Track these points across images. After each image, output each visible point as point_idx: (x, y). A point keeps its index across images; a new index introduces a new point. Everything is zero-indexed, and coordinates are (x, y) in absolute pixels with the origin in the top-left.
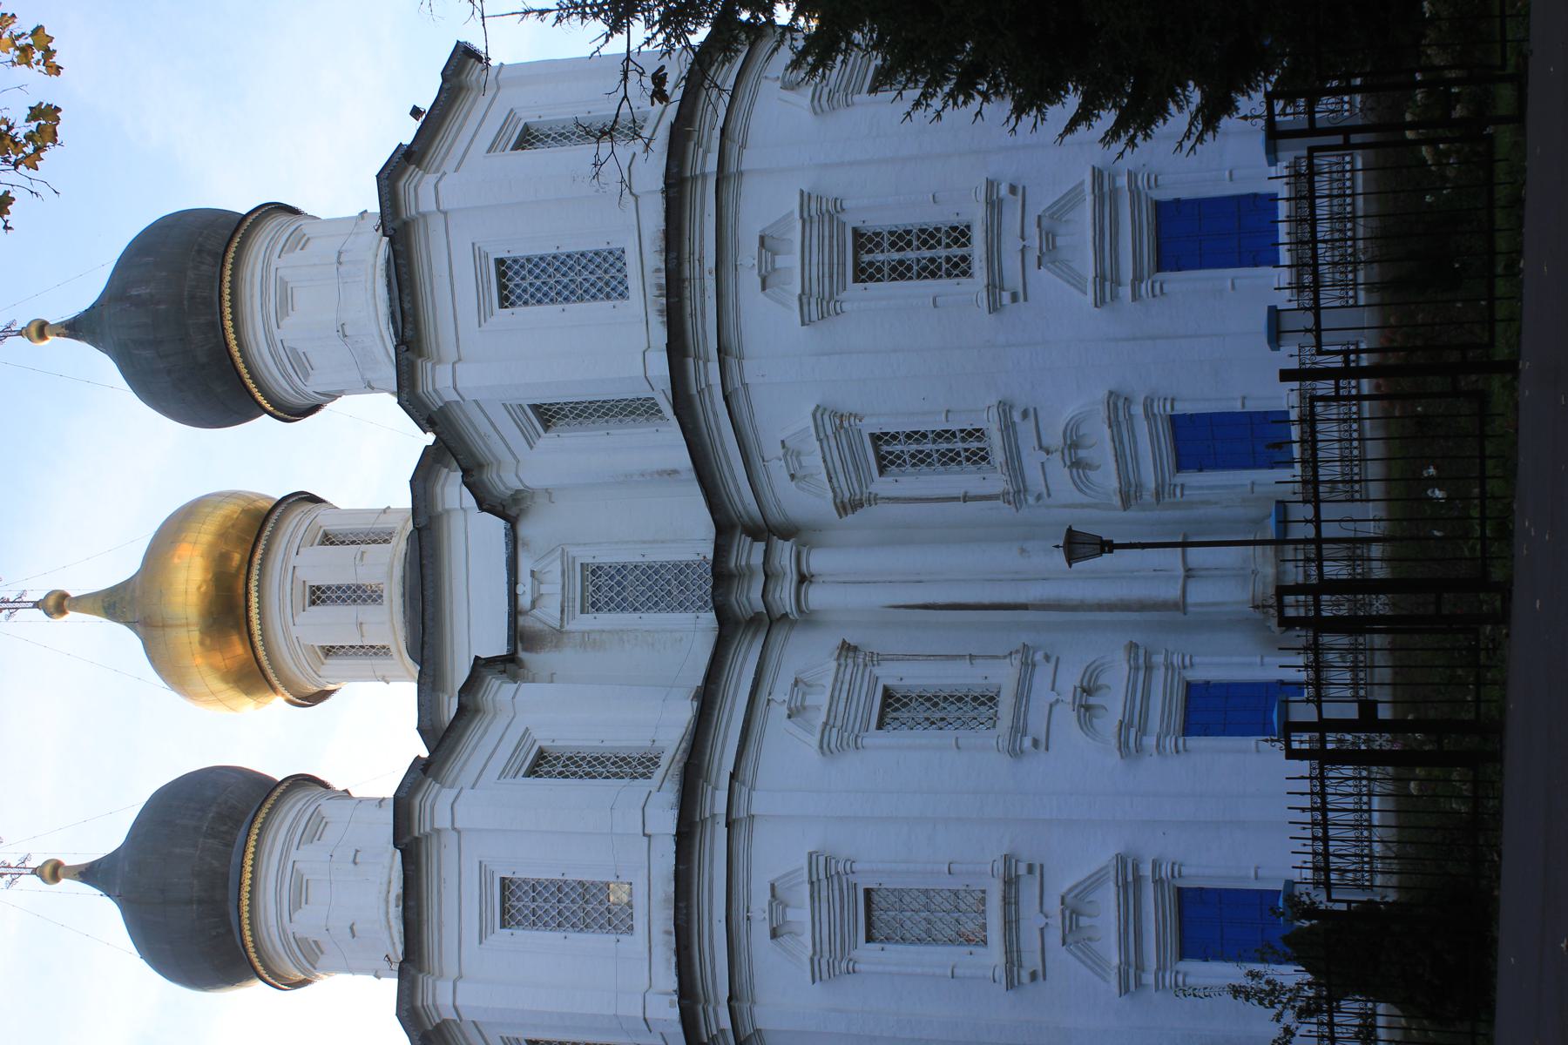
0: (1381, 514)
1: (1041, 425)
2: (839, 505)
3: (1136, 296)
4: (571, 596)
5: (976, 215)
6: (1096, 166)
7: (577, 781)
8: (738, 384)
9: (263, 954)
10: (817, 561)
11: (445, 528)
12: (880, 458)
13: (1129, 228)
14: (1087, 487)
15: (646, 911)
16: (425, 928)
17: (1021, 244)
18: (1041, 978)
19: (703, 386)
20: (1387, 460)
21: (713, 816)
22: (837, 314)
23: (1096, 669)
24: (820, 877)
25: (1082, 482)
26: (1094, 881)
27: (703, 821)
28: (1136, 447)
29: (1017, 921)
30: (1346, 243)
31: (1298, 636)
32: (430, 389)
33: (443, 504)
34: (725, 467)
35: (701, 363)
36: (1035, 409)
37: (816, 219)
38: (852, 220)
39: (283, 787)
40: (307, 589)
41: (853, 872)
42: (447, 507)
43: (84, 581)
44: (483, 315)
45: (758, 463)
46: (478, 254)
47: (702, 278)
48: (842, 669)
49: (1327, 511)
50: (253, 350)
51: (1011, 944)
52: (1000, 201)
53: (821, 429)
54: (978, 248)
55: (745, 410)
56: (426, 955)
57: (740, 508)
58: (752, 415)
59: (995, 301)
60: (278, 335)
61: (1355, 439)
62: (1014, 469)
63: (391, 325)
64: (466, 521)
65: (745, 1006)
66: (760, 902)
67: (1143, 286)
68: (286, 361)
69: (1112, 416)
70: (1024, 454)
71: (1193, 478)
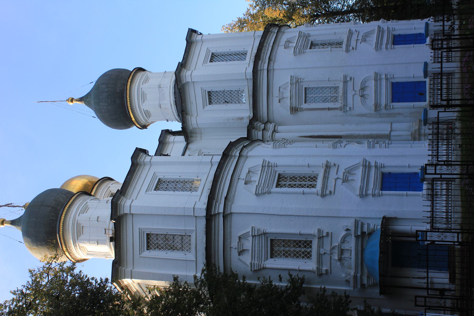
1: (355, 83)
2: (291, 108)
3: (387, 48)
5: (341, 85)
6: (376, 72)
8: (272, 68)
9: (64, 226)
10: (280, 128)
11: (166, 147)
13: (386, 37)
14: (364, 104)
15: (204, 183)
16: (130, 187)
18: (333, 193)
19: (262, 69)
22: (304, 53)
23: (364, 81)
24: (266, 165)
25: (364, 102)
28: (381, 90)
29: (328, 178)
30: (448, 191)
32: (184, 74)
35: (263, 63)
36: (354, 78)
37: (302, 36)
38: (311, 39)
40: (111, 193)
42: (169, 141)
44: (204, 62)
45: (271, 95)
46: (208, 50)
47: (268, 47)
50: (133, 90)
51: (325, 183)
53: (292, 81)
56: (126, 195)
59: (348, 48)
60: (141, 86)
61: (450, 201)
62: (345, 97)
63: (174, 83)
64: (173, 145)
65: (230, 203)
66: (245, 171)
67: (389, 45)
68: (140, 96)
69: (376, 76)
70: (348, 92)
71: (396, 105)
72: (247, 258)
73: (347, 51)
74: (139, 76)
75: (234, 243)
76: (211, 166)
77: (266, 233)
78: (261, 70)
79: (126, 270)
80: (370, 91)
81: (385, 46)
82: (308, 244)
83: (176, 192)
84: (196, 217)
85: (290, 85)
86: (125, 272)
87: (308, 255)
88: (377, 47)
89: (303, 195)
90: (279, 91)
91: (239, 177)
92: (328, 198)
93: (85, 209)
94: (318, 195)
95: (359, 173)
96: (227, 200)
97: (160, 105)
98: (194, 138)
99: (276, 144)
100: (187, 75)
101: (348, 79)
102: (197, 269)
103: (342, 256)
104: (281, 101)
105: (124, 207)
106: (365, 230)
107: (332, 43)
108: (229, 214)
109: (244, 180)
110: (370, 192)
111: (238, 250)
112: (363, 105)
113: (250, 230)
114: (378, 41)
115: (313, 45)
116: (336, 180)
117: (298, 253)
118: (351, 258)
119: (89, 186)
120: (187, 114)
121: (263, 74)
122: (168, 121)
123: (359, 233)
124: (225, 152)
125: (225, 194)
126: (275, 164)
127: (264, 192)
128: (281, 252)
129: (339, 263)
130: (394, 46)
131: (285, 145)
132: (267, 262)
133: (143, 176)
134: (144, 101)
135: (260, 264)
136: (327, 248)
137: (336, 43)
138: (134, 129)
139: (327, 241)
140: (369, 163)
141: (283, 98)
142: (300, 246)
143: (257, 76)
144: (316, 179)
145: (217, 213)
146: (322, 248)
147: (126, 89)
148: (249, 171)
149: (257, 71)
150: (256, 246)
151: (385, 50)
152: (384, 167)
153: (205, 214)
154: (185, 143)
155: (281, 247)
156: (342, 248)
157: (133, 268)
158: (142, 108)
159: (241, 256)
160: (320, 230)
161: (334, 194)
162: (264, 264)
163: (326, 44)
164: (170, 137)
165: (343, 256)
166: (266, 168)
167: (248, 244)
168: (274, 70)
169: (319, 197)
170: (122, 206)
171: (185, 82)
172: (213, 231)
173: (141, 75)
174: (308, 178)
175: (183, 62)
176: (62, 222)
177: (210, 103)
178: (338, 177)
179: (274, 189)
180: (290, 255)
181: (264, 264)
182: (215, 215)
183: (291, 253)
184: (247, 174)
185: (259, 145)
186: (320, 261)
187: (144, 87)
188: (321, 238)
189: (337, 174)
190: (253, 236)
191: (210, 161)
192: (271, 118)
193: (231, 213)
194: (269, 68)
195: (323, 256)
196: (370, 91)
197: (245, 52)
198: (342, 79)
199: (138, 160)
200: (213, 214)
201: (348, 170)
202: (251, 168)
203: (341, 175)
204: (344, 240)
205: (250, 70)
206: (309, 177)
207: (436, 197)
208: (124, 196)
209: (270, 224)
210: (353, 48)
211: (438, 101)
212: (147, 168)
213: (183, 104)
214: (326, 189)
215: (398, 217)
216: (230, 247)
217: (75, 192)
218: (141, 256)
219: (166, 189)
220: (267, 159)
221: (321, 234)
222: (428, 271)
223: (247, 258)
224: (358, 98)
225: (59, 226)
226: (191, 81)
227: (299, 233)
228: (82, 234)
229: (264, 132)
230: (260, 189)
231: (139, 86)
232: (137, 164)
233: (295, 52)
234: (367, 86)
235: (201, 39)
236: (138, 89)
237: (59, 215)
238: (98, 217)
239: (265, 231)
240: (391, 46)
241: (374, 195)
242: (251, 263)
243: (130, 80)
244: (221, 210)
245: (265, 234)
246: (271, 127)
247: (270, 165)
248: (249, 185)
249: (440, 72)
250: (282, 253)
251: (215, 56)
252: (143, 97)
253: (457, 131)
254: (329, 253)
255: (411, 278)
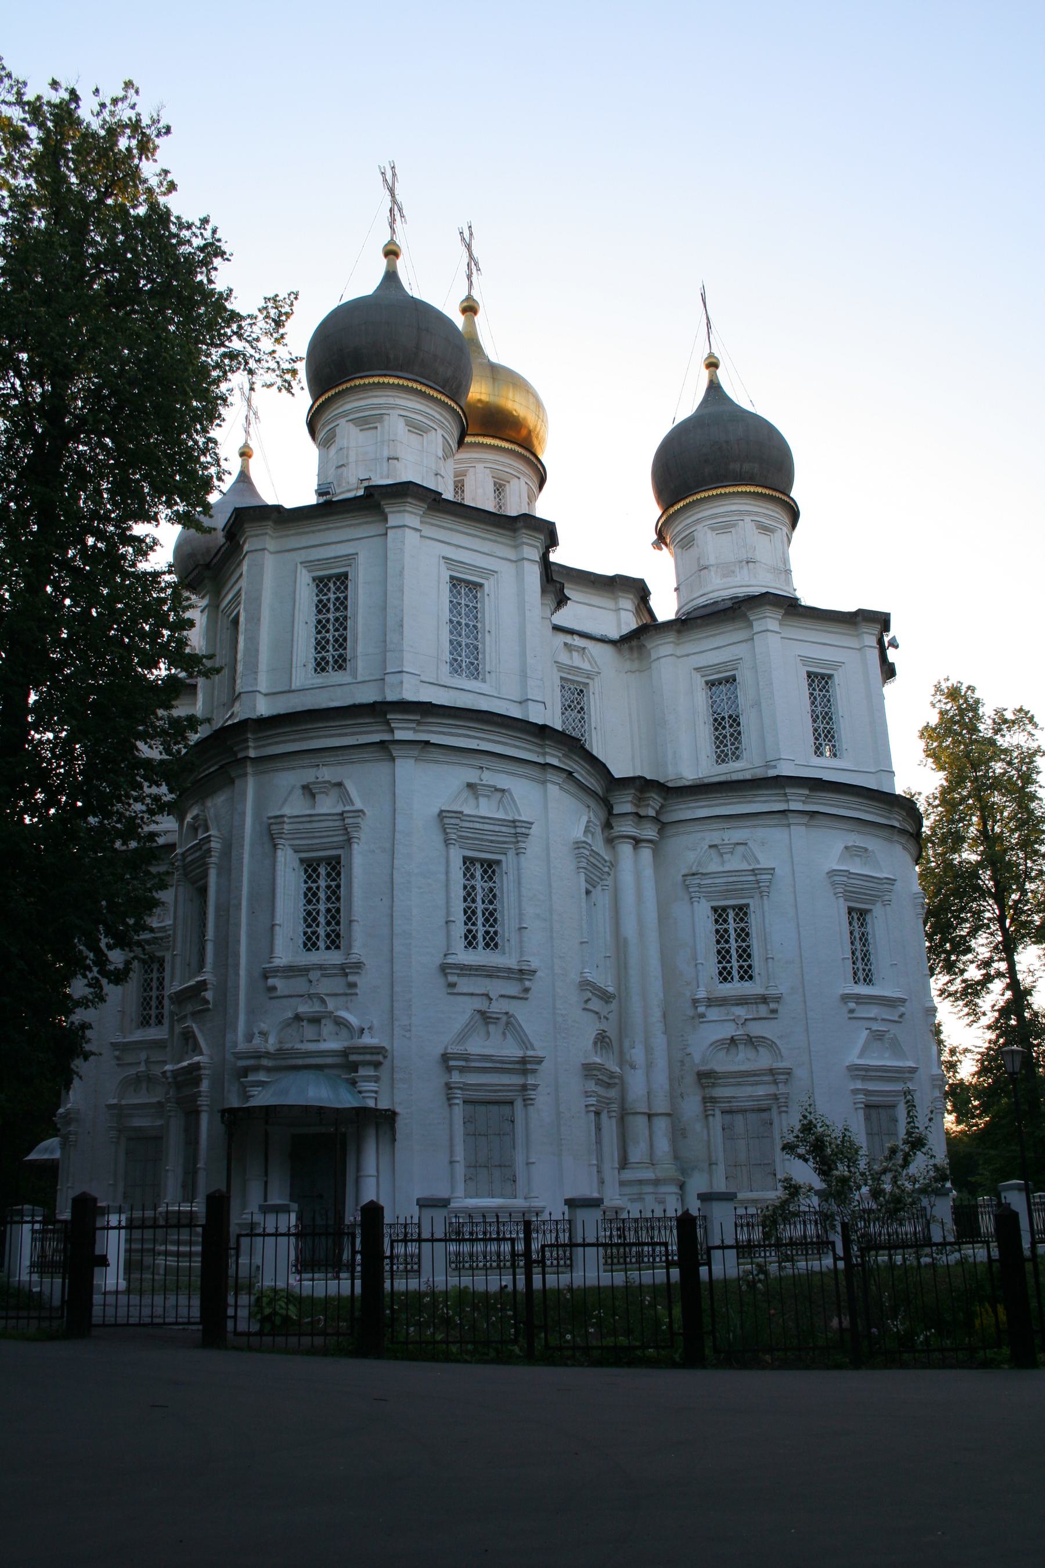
0: (589, 1283)
3: (855, 1092)
4: (572, 672)
7: (807, 693)
12: (724, 909)
17: (880, 1018)
19: (789, 797)
20: (570, 1289)
21: (544, 754)
22: (835, 894)
26: (524, 1043)
27: (542, 746)
31: (564, 1214)
33: (623, 597)
34: (722, 801)
35: (804, 798)
36: (776, 1018)
39: (786, 499)
41: (517, 854)
43: (723, 376)
44: (805, 660)
48: (603, 862)
49: (439, 1246)
51: (476, 970)
52: (894, 1007)
54: (736, 988)
55: (768, 822)
57: (673, 808)
58: (763, 826)
60: (748, 519)
65: (416, 753)
66: (502, 781)
72: (295, 807)
73: (845, 998)
74: (773, 511)
75: (326, 774)
76: (518, 700)
77: (350, 844)
78: (785, 795)
79: (267, 537)
80: (743, 1060)
81: (860, 1087)
82: (334, 941)
83: (446, 629)
84: (383, 679)
85: (751, 868)
86: (262, 534)
87: (310, 943)
88: (857, 1069)
89: (442, 922)
90: (738, 844)
91: (487, 768)
92: (441, 981)
93: (416, 428)
94: (445, 955)
95: (511, 1050)
96: (423, 748)
97: (705, 568)
98: (627, 656)
99: (584, 848)
100: (769, 621)
101: (772, 1006)
102: (273, 696)
103: (305, 1021)
104: (713, 851)
105: (399, 512)
106: (363, 1072)
107: (868, 960)
108: (391, 755)
109: (478, 781)
110: (456, 1077)
111: (314, 783)
112: (711, 1045)
113: (358, 805)
114: (873, 1070)
115: (861, 915)
116: (487, 995)
117: (315, 919)
118: (302, 1041)
119: (519, 431)
120: (679, 632)
121: (775, 801)
122: (676, 589)
123: (353, 1058)
124: (249, 721)
125: (434, 739)
126: (524, 851)
127: (448, 830)
128: (315, 881)
129: (290, 1015)
130: (861, 1108)
131: (581, 870)
132: (290, 852)
133: (487, 546)
134: (713, 529)
135: (283, 836)
136: (325, 986)
137: (870, 970)
138: (654, 511)
139: (336, 984)
140: (534, 1071)
141: (721, 855)
142: (328, 923)
143: (767, 788)
144: (492, 949)
145: (393, 725)
146: (323, 976)
147: (736, 485)
148: (503, 791)
149: (783, 787)
150: (323, 824)
151: (852, 1088)
152: (525, 1106)
153: (389, 699)
154: (615, 635)
155: (326, 881)
156: (323, 1022)
157: (272, 553)
158: (699, 527)
159: (300, 791)
160: (359, 968)
161: (448, 994)
162: (284, 845)
163: (864, 945)
164: (632, 600)
165: (305, 1023)
166: (513, 831)
167: (327, 805)
168: (789, 825)
169: (438, 960)
170: (402, 508)
171: (751, 618)
172: (489, 729)
173: (776, 515)
174: (492, 930)
175: (801, 610)
176: (381, 380)
177: (711, 684)
178: (491, 999)
179: (456, 856)
180: (309, 902)
181: (284, 845)
182: (387, 723)
183: (314, 905)
184: (494, 787)
185: (589, 807)
186: (292, 971)
187: (747, 526)
188: (344, 970)
189: (502, 996)
190: (342, 814)
191: (529, 697)
192: (670, 831)
193: (393, 759)
194: (790, 815)
195: (304, 979)
196: (743, 1060)
197: (838, 754)
198: (772, 991)
199: (524, 531)
200: (388, 717)
201: (514, 1021)
202: (511, 794)
203: (498, 1007)
204: (340, 1023)
205: (786, 770)
206: (496, 933)
207: (412, 1235)
208: (430, 508)
209: (374, 851)
210: (852, 1011)
211: (665, 1228)
212: (511, 554)
213: (699, 621)
214: (459, 975)
215: (396, 1143)
216: (318, 765)
217: (792, 495)
218: (299, 566)
219: (454, 606)
220: (534, 830)
221: (351, 971)
222: (123, 1228)
223: (295, 807)
224: (729, 1031)
225: (373, 376)
226: (755, 631)
227: (353, 918)
228: (361, 430)
229: (631, 817)
230: (453, 821)
231: (749, 513)
232: (514, 530)
233: (835, 873)
234: (758, 1051)
235: (866, 646)
236: (740, 513)
237: (401, 371)
238: (397, 459)
239: (355, 840)
240: (862, 1102)
241: (449, 1086)
242: (282, 816)
243: (760, 490)
244: (399, 735)
245: (349, 841)
246: (650, 832)
247: (519, 839)
248: (466, 793)
249: (574, 1241)
250: (312, 885)
251: (827, 683)
252: (724, 528)
253: (634, 1275)
254: (312, 992)
255: (265, 1179)
